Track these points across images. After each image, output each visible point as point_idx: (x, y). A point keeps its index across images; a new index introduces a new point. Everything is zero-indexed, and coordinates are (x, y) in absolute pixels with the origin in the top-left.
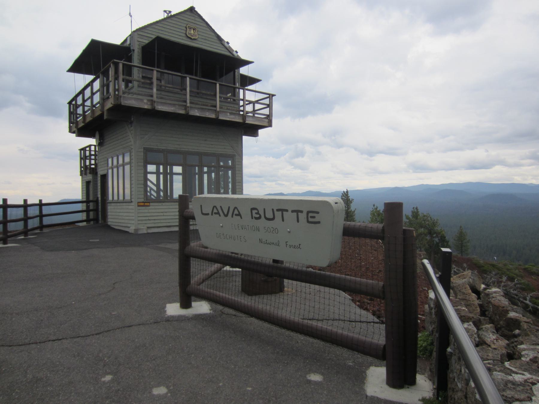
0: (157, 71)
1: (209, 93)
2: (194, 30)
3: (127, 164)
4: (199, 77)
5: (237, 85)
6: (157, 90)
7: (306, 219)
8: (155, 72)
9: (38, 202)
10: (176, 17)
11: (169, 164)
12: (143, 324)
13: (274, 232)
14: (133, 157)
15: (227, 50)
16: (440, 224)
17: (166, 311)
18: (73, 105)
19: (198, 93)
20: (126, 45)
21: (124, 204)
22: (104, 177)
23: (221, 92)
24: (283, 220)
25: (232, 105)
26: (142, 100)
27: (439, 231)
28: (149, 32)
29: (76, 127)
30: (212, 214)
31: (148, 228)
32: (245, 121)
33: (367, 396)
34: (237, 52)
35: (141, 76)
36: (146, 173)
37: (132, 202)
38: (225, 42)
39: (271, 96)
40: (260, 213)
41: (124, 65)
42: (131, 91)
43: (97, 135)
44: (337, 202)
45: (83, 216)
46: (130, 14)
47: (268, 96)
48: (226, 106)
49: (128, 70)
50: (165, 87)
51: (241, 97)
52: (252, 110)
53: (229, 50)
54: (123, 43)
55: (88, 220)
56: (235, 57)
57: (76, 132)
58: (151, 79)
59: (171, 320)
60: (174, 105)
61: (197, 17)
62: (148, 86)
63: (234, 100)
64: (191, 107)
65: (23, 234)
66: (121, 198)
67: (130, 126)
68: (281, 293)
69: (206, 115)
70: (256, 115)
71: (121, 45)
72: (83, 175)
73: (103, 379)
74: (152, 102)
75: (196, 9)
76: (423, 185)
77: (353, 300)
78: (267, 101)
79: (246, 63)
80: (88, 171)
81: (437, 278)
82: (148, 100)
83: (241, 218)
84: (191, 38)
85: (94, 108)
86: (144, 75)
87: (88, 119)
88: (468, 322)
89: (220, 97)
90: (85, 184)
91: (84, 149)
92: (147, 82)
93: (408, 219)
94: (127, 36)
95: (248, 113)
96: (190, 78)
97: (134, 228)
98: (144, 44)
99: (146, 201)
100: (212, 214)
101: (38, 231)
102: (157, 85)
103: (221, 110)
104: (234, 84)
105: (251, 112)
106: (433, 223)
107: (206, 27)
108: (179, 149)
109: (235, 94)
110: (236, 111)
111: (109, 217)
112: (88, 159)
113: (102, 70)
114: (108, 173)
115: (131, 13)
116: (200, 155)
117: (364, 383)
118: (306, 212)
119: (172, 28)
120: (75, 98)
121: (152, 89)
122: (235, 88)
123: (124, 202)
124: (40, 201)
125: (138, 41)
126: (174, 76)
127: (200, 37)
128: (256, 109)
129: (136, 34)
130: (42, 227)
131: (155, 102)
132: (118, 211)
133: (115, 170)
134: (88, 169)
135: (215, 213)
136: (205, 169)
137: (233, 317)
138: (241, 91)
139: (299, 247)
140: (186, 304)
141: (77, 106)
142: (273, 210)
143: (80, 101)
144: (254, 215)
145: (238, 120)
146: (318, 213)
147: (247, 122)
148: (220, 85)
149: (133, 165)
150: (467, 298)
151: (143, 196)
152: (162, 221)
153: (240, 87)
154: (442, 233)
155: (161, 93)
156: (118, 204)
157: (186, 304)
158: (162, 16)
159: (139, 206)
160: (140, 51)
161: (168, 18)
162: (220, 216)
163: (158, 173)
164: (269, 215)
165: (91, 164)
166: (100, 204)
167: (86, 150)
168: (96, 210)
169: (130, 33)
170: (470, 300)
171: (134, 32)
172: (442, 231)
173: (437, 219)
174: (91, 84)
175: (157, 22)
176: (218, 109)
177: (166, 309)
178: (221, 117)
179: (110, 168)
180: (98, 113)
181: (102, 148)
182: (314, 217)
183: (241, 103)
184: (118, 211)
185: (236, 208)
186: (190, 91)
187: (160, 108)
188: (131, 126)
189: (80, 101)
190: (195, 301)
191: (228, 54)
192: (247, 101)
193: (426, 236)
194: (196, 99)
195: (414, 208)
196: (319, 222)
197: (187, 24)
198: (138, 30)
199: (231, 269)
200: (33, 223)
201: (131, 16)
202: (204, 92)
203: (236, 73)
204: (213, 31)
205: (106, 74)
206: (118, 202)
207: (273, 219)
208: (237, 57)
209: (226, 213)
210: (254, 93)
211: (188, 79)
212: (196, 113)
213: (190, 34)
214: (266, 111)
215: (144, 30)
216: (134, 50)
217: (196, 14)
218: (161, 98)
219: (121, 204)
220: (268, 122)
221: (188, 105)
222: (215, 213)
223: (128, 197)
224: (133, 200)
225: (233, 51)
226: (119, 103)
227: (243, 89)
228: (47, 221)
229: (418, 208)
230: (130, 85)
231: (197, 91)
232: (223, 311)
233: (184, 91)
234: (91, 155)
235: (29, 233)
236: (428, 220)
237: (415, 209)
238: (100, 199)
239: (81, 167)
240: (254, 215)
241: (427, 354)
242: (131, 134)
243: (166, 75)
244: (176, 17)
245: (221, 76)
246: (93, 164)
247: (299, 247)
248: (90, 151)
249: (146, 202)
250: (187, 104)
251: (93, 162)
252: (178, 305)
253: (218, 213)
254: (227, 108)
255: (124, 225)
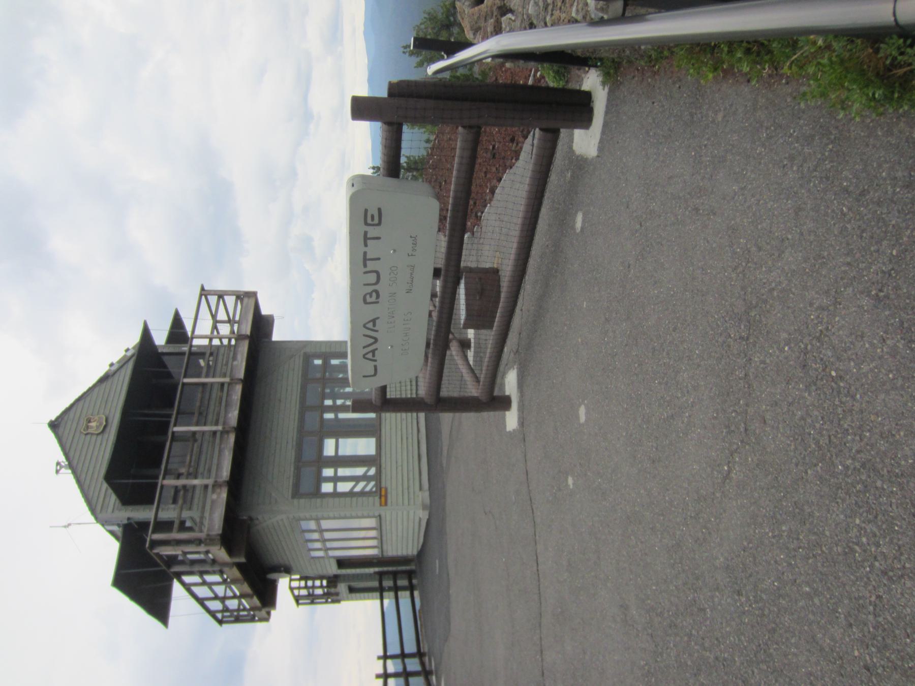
0: (164, 478)
1: (199, 395)
2: (89, 421)
3: (319, 525)
4: (173, 411)
5: (185, 349)
6: (196, 478)
7: (375, 227)
8: (166, 482)
9: (381, 662)
10: (69, 451)
11: (323, 461)
12: (525, 456)
13: (395, 272)
14: (308, 515)
15: (125, 367)
16: (432, 9)
17: (514, 430)
18: (223, 617)
19: (200, 414)
20: (120, 534)
21: (384, 528)
22: (342, 563)
23: (199, 376)
24: (379, 259)
25: (220, 357)
26: (213, 502)
27: (445, 9)
28: (96, 494)
29: (259, 609)
30: (375, 361)
31: (421, 489)
32: (248, 335)
33: (598, 156)
34: (127, 350)
35: (173, 506)
36: (335, 494)
37: (380, 516)
38: (109, 370)
39: (204, 293)
40: (370, 291)
41: (153, 532)
42: (198, 520)
43: (272, 576)
44: (351, 185)
45: (405, 597)
46: (65, 527)
47: (203, 297)
48: (222, 366)
49: (163, 526)
50: (190, 466)
51: (205, 342)
52: (228, 325)
53: (124, 362)
54: (117, 538)
55: (411, 588)
56: (136, 353)
57: (267, 609)
58: (176, 489)
59: (522, 422)
60: (221, 451)
61: (67, 416)
62: (190, 494)
63: (211, 354)
64: (224, 423)
65: (429, 677)
66: (373, 533)
67: (256, 522)
68: (500, 273)
69: (237, 399)
70: (237, 318)
71: (121, 539)
72: (339, 598)
73: (571, 487)
74: (216, 485)
75: (53, 419)
76: (365, 33)
77: (511, 168)
78: (213, 299)
79: (146, 335)
80: (333, 590)
81: (448, 57)
82: (213, 492)
83: (378, 318)
84: (105, 427)
85: (229, 580)
86: (171, 501)
87: (247, 589)
88: (501, 23)
89: (207, 376)
90: (353, 595)
91: (297, 599)
92: (182, 495)
93: (423, 64)
94: (104, 531)
95: (232, 332)
96: (175, 425)
97: (421, 511)
98: (118, 501)
99: (379, 492)
100: (375, 361)
101: (426, 659)
102: (187, 478)
103: (228, 373)
104: (183, 354)
105: (232, 327)
106: (430, 19)
107: (85, 401)
108: (294, 443)
109: (201, 353)
110: (230, 351)
111: (405, 553)
112: (313, 591)
113: (164, 568)
114: (334, 557)
115: (64, 525)
116: (304, 408)
117: (587, 159)
118: (366, 227)
119: (89, 457)
120: (212, 614)
121: (194, 487)
122: (191, 354)
123: (380, 528)
124: (379, 658)
125: (113, 512)
126: (172, 453)
127: (102, 411)
128: (226, 318)
129: (100, 516)
130: (420, 654)
131: (216, 482)
132: (394, 538)
133: (329, 545)
134: (329, 590)
135: (374, 356)
136: (328, 402)
137: (521, 336)
138: (196, 342)
139: (414, 239)
140: (504, 403)
141: (226, 609)
142: (365, 273)
143: (215, 605)
144: (374, 299)
145: (244, 347)
146: (366, 211)
147: (248, 333)
148: (185, 377)
149: (320, 514)
150: (484, 14)
151: (371, 499)
152: (411, 467)
153: (188, 345)
154: (448, 6)
155: (201, 474)
156: (384, 538)
157: (504, 403)
158: (68, 477)
159: (386, 504)
160: (130, 508)
161: (71, 466)
162: (377, 349)
163: (336, 479)
164: (372, 278)
165: (322, 587)
166: (385, 569)
167: (299, 596)
168: (395, 575)
169: (99, 526)
170: (487, 12)
171: (96, 518)
172: (446, 6)
173: (424, 13)
174: (187, 587)
175: (79, 482)
176: (227, 380)
177: (511, 430)
178: (241, 374)
179: (327, 554)
180: (236, 573)
181: (294, 568)
182: (373, 217)
183: (216, 342)
184: (394, 538)
185: (364, 326)
186: (197, 424)
187: (225, 472)
188: (257, 519)
189: (215, 605)
190: (504, 392)
191: (130, 366)
192: (212, 332)
193: (453, 33)
194: (210, 417)
195: (404, 52)
196: (380, 210)
197: (81, 433)
198: (93, 511)
199: (472, 349)
200: (413, 665)
201: (69, 525)
202: (198, 404)
203: (165, 351)
204: (91, 389)
205: (172, 561)
206: (381, 539)
207: (377, 273)
208: (137, 348)
209: (373, 340)
210: (198, 321)
211: (176, 429)
212: (233, 416)
213: (98, 427)
214: (230, 300)
215: (94, 502)
216: (129, 519)
217: (62, 419)
218: (210, 471)
219: (384, 533)
220: (247, 297)
221: (220, 428)
222: (374, 356)
223: (371, 522)
224: (377, 514)
225: (125, 356)
226: (219, 537)
227: (192, 338)
228: (411, 647)
229: (405, 45)
230: (188, 524)
231: (196, 415)
232: (515, 351)
233: (197, 436)
234: (306, 587)
235: (428, 668)
236: (425, 28)
237: (405, 50)
238: (377, 569)
239: (327, 602)
240: (374, 299)
241: (563, 71)
242: (270, 519)
243: (170, 467)
244: (69, 451)
245: (169, 375)
246: (322, 583)
247: (414, 239)
248: (299, 588)
249: (381, 494)
250: (219, 431)
251: (318, 583)
252: (507, 413)
253: (373, 352)
254: (225, 365)
255: (416, 530)
